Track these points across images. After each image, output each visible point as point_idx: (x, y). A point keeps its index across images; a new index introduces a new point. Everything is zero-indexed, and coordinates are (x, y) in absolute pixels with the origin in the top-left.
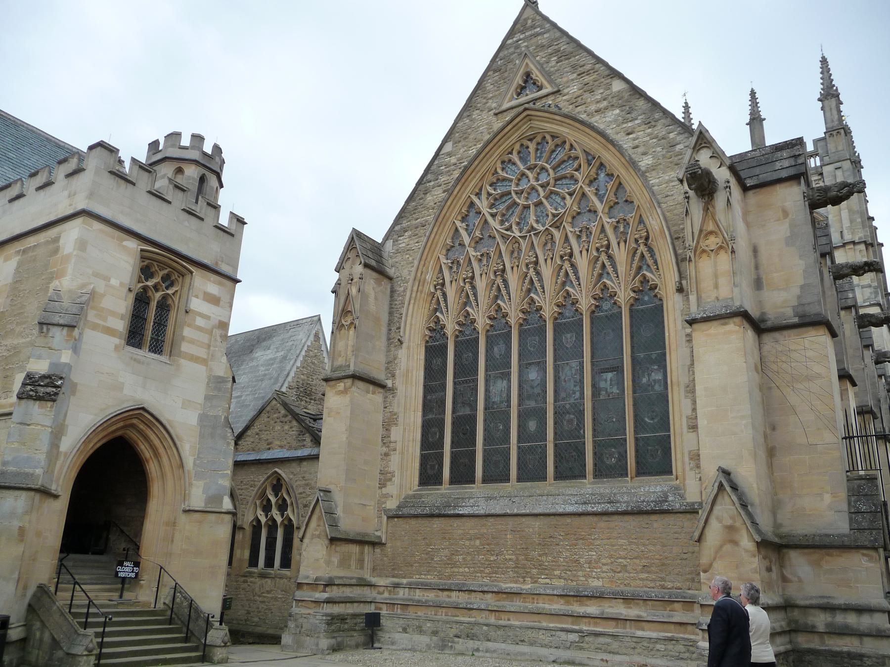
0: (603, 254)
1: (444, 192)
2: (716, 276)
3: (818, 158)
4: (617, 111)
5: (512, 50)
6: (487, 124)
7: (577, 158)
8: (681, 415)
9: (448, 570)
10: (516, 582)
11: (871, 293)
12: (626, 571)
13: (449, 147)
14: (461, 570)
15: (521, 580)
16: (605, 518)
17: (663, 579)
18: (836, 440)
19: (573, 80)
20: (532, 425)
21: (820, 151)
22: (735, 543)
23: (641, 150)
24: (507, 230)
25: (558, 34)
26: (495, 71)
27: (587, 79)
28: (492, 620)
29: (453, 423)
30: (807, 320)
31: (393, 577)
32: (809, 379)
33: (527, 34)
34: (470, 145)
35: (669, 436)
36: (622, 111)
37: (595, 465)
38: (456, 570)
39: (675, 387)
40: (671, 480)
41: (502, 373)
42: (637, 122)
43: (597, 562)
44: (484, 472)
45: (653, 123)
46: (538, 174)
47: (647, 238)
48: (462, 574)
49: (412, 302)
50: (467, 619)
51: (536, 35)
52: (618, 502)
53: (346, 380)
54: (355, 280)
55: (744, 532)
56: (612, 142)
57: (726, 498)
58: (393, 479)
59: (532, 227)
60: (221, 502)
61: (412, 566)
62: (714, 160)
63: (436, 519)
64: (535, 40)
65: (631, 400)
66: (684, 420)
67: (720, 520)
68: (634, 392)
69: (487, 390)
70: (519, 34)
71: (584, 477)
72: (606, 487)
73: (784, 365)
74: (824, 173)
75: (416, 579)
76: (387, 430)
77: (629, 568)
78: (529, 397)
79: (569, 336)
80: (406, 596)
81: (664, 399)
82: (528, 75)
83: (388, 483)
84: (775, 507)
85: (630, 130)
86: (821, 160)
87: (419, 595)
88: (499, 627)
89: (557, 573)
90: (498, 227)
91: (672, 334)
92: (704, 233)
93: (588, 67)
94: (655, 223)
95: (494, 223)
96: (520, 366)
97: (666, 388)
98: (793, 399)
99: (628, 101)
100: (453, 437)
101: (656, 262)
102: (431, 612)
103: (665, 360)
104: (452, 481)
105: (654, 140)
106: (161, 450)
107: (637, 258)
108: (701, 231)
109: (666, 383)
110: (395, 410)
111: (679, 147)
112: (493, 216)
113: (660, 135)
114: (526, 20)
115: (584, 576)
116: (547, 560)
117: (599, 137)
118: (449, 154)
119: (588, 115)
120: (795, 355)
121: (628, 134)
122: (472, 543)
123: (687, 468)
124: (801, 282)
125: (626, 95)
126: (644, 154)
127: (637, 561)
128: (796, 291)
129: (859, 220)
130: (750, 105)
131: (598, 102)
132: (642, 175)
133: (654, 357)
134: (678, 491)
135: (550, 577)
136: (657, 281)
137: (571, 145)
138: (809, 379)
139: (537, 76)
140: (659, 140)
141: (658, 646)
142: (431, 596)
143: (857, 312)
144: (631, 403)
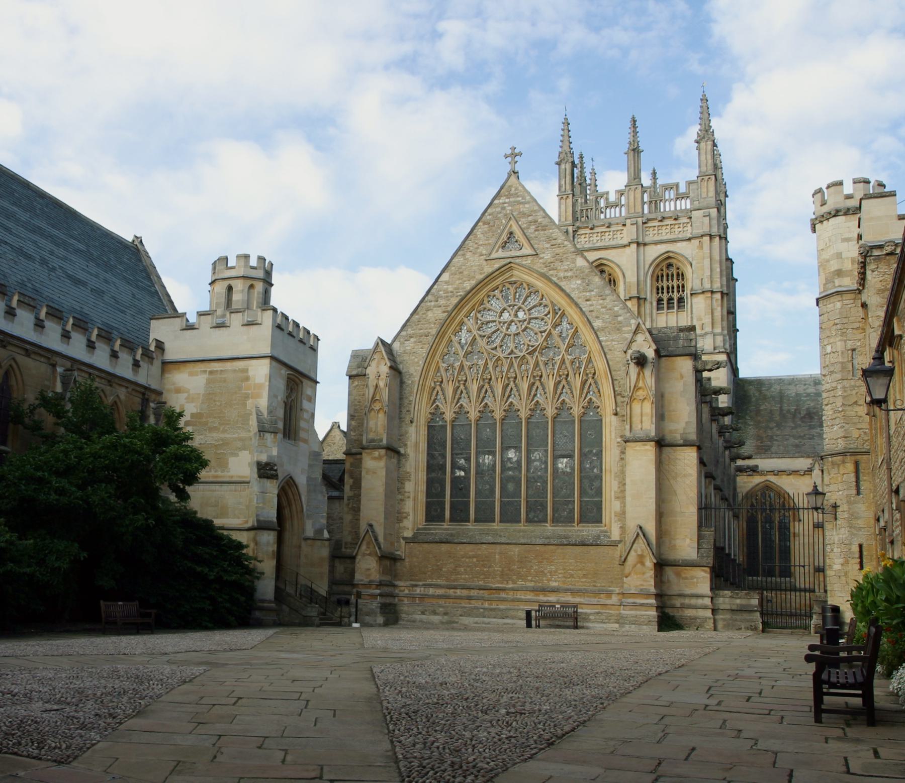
0: (564, 380)
1: (444, 312)
3: (688, 201)
4: (579, 282)
5: (498, 209)
6: (479, 265)
8: (611, 491)
10: (502, 583)
12: (573, 577)
14: (463, 576)
16: (561, 547)
17: (595, 582)
19: (547, 248)
21: (691, 195)
22: (643, 564)
25: (536, 208)
26: (485, 223)
27: (558, 251)
28: (486, 605)
30: (688, 443)
33: (511, 200)
34: (465, 279)
36: (583, 282)
39: (607, 472)
40: (602, 527)
42: (593, 293)
45: (604, 297)
46: (517, 312)
47: (594, 374)
48: (464, 579)
49: (419, 393)
50: (468, 605)
51: (519, 203)
53: (380, 450)
54: (381, 377)
55: (648, 558)
56: (577, 305)
61: (425, 574)
62: (646, 343)
63: (443, 544)
64: (517, 207)
66: (613, 493)
67: (636, 551)
71: (547, 522)
72: (560, 529)
75: (429, 581)
77: (575, 576)
78: (510, 469)
80: (422, 592)
83: (404, 520)
85: (588, 298)
87: (431, 591)
88: (491, 610)
89: (530, 578)
91: (608, 440)
92: (637, 388)
93: (560, 241)
96: (502, 448)
97: (602, 472)
99: (587, 275)
102: (441, 602)
104: (452, 520)
105: (604, 309)
106: (293, 501)
108: (635, 386)
110: (408, 470)
111: (620, 318)
113: (608, 307)
114: (510, 187)
115: (547, 580)
118: (447, 283)
119: (558, 279)
121: (587, 300)
122: (471, 560)
123: (613, 521)
124: (686, 420)
126: (597, 317)
127: (580, 572)
130: (629, 133)
131: (565, 271)
134: (607, 534)
135: (525, 580)
137: (543, 295)
142: (440, 592)
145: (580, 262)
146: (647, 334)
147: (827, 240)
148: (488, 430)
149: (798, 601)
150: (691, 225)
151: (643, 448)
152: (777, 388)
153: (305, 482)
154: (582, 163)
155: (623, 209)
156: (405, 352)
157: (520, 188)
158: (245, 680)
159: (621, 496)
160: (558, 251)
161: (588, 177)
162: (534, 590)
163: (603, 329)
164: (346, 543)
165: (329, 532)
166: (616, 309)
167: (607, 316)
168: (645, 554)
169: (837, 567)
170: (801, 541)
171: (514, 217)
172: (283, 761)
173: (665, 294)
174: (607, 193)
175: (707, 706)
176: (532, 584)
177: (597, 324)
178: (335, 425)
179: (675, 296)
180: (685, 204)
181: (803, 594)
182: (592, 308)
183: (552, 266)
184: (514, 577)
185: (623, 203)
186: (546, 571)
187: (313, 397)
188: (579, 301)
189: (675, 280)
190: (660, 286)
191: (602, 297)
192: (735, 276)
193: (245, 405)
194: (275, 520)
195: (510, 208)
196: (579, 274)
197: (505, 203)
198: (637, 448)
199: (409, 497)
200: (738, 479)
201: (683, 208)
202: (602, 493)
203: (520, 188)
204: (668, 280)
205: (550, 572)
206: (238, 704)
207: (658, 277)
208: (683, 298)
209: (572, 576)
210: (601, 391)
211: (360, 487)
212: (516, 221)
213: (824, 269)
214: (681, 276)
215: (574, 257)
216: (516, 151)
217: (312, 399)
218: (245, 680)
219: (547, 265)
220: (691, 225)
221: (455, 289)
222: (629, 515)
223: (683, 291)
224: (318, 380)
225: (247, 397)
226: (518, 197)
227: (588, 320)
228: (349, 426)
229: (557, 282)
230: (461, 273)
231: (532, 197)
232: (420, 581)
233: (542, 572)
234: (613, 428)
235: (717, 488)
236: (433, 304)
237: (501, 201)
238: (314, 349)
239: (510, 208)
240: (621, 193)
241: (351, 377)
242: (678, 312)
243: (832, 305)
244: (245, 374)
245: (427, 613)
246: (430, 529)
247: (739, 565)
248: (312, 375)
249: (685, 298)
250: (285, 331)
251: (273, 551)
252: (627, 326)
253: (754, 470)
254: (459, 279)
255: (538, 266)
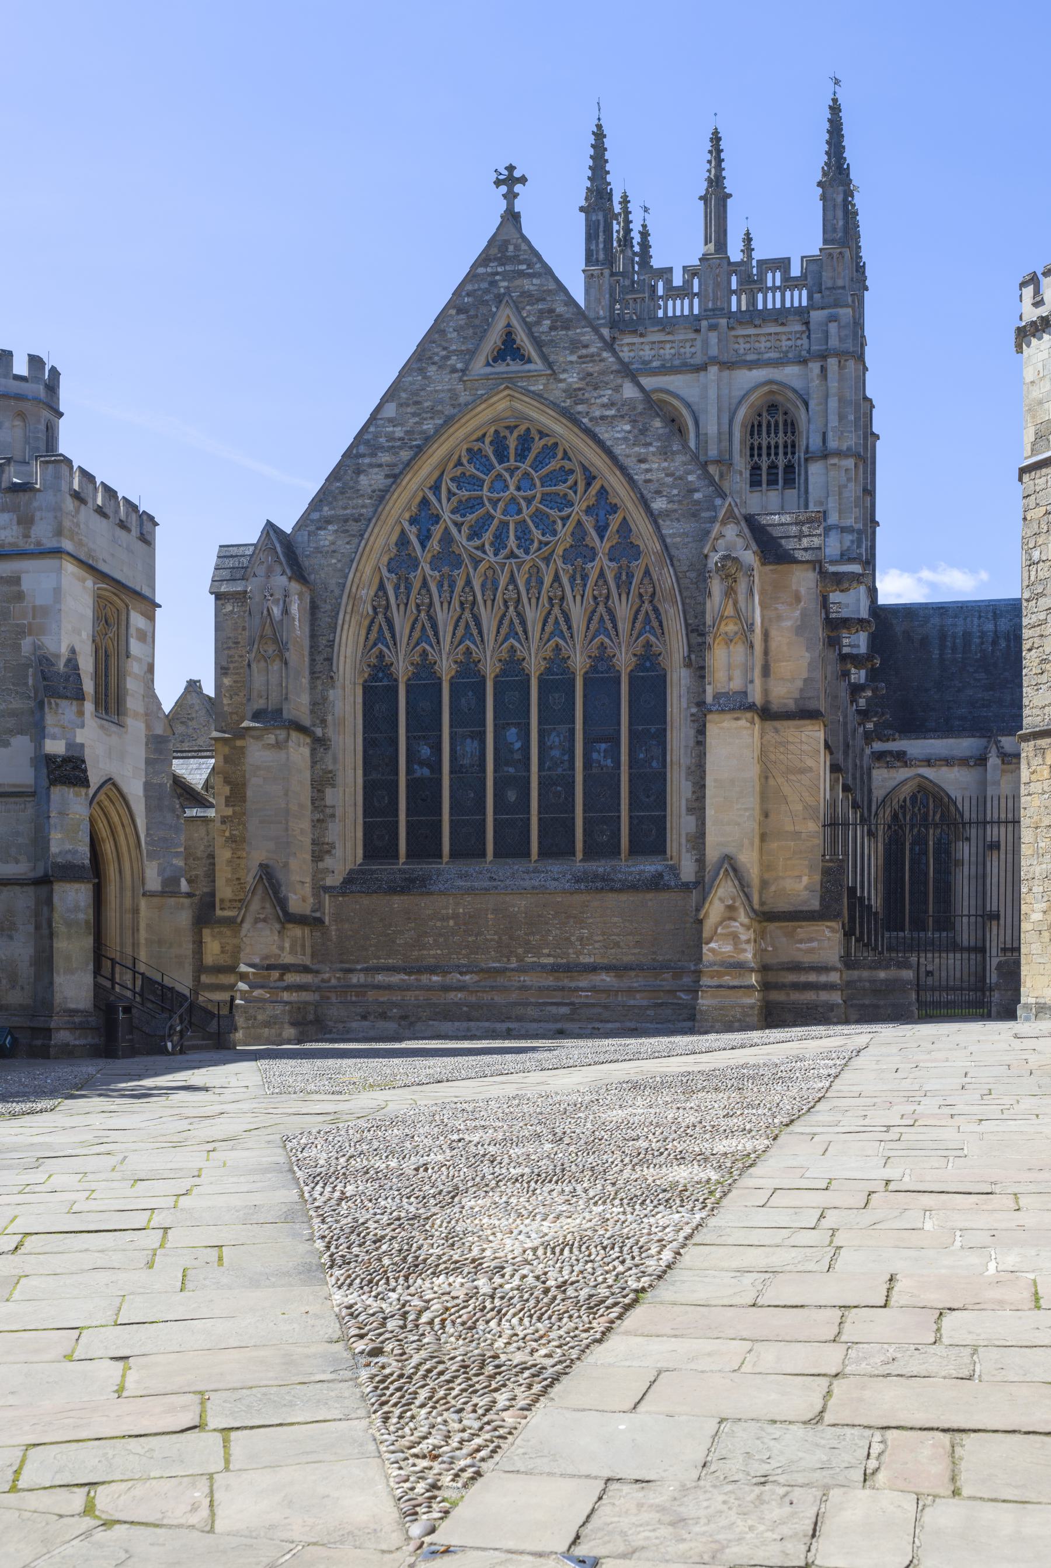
2: (729, 667)
6: (449, 390)
7: (572, 471)
9: (416, 953)
11: (852, 542)
12: (619, 947)
13: (390, 410)
14: (432, 952)
15: (505, 959)
18: (817, 829)
20: (512, 796)
23: (653, 487)
24: (477, 548)
25: (552, 286)
27: (590, 367)
29: (408, 786)
31: (341, 962)
32: (802, 771)
33: (508, 268)
35: (665, 816)
37: (585, 842)
38: (425, 952)
39: (675, 767)
41: (472, 732)
42: (652, 449)
43: (588, 939)
44: (451, 845)
47: (654, 594)
51: (521, 274)
52: (613, 880)
55: (742, 911)
56: (623, 469)
57: (730, 883)
58: (334, 851)
59: (512, 552)
60: (179, 885)
65: (627, 775)
66: (684, 802)
67: (721, 900)
68: (630, 767)
69: (453, 750)
70: (495, 264)
73: (782, 757)
74: (811, 324)
76: (319, 791)
77: (622, 944)
79: (557, 695)
81: (661, 777)
82: (509, 337)
84: (764, 884)
85: (642, 457)
86: (810, 297)
89: (546, 951)
90: (464, 542)
93: (593, 350)
94: (666, 578)
95: (461, 538)
97: (665, 767)
98: (786, 790)
100: (408, 803)
101: (661, 625)
103: (665, 736)
107: (641, 617)
109: (665, 760)
110: (330, 768)
111: (697, 496)
112: (458, 525)
113: (677, 474)
116: (535, 939)
117: (604, 456)
120: (791, 747)
122: (445, 924)
123: (684, 850)
124: (805, 675)
125: (640, 407)
126: (658, 492)
127: (630, 938)
128: (799, 684)
129: (852, 417)
132: (653, 517)
133: (653, 730)
134: (674, 870)
135: (539, 955)
136: (661, 648)
138: (802, 771)
139: (522, 341)
140: (675, 479)
141: (648, 1012)
143: (840, 650)
144: (627, 779)
145: (629, 391)
146: (743, 524)
147: (1040, 366)
148: (470, 693)
149: (958, 967)
150: (809, 337)
151: (735, 724)
152: (936, 620)
153: (140, 792)
154: (627, 212)
155: (696, 301)
156: (318, 550)
157: (524, 247)
158: (38, 1188)
159: (697, 806)
160: (590, 367)
161: (637, 238)
162: (555, 969)
163: (667, 514)
164: (222, 901)
165: (190, 881)
166: (691, 478)
167: (675, 492)
168: (737, 904)
169: (1036, 916)
170: (966, 873)
171: (514, 302)
172: (120, 1391)
173: (764, 457)
174: (670, 270)
175: (888, 1182)
176: (551, 960)
177: (659, 504)
178: (193, 686)
179: (781, 461)
180: (799, 298)
181: (965, 955)
182: (648, 476)
183: (580, 396)
184: (520, 951)
185: (696, 290)
186: (573, 938)
187: (149, 635)
188: (630, 463)
189: (781, 434)
190: (756, 444)
191: (665, 453)
192: (875, 430)
193: (17, 647)
194: (87, 862)
195: (505, 284)
196: (625, 411)
197: (497, 273)
198: (725, 724)
199: (333, 816)
200: (875, 773)
201: (796, 304)
202: (665, 803)
203: (524, 247)
204: (768, 433)
205: (581, 939)
206: (23, 1250)
207: (753, 426)
208: (793, 466)
209: (617, 945)
210: (665, 623)
211: (243, 799)
212: (517, 308)
213: (1034, 417)
214: (791, 426)
215: (619, 381)
216: (517, 174)
217: (148, 638)
218: (38, 1188)
219: (571, 393)
220: (809, 337)
221: (407, 432)
222: (711, 839)
223: (793, 453)
224: (158, 600)
225: (21, 632)
226: (521, 263)
227: (642, 496)
228: (218, 687)
229: (589, 425)
230: (417, 403)
231: (545, 265)
232: (358, 962)
233: (568, 939)
234: (684, 690)
235: (846, 789)
236: (367, 460)
237: (489, 270)
238: (147, 540)
239: (505, 284)
240: (690, 272)
241: (219, 597)
242: (784, 488)
243: (1044, 479)
244: (15, 588)
245: (372, 1018)
246: (373, 872)
247: (876, 913)
248: (146, 591)
249: (796, 466)
250: (90, 504)
251: (87, 922)
252: (708, 509)
253: (901, 758)
254: (414, 415)
255: (556, 392)
